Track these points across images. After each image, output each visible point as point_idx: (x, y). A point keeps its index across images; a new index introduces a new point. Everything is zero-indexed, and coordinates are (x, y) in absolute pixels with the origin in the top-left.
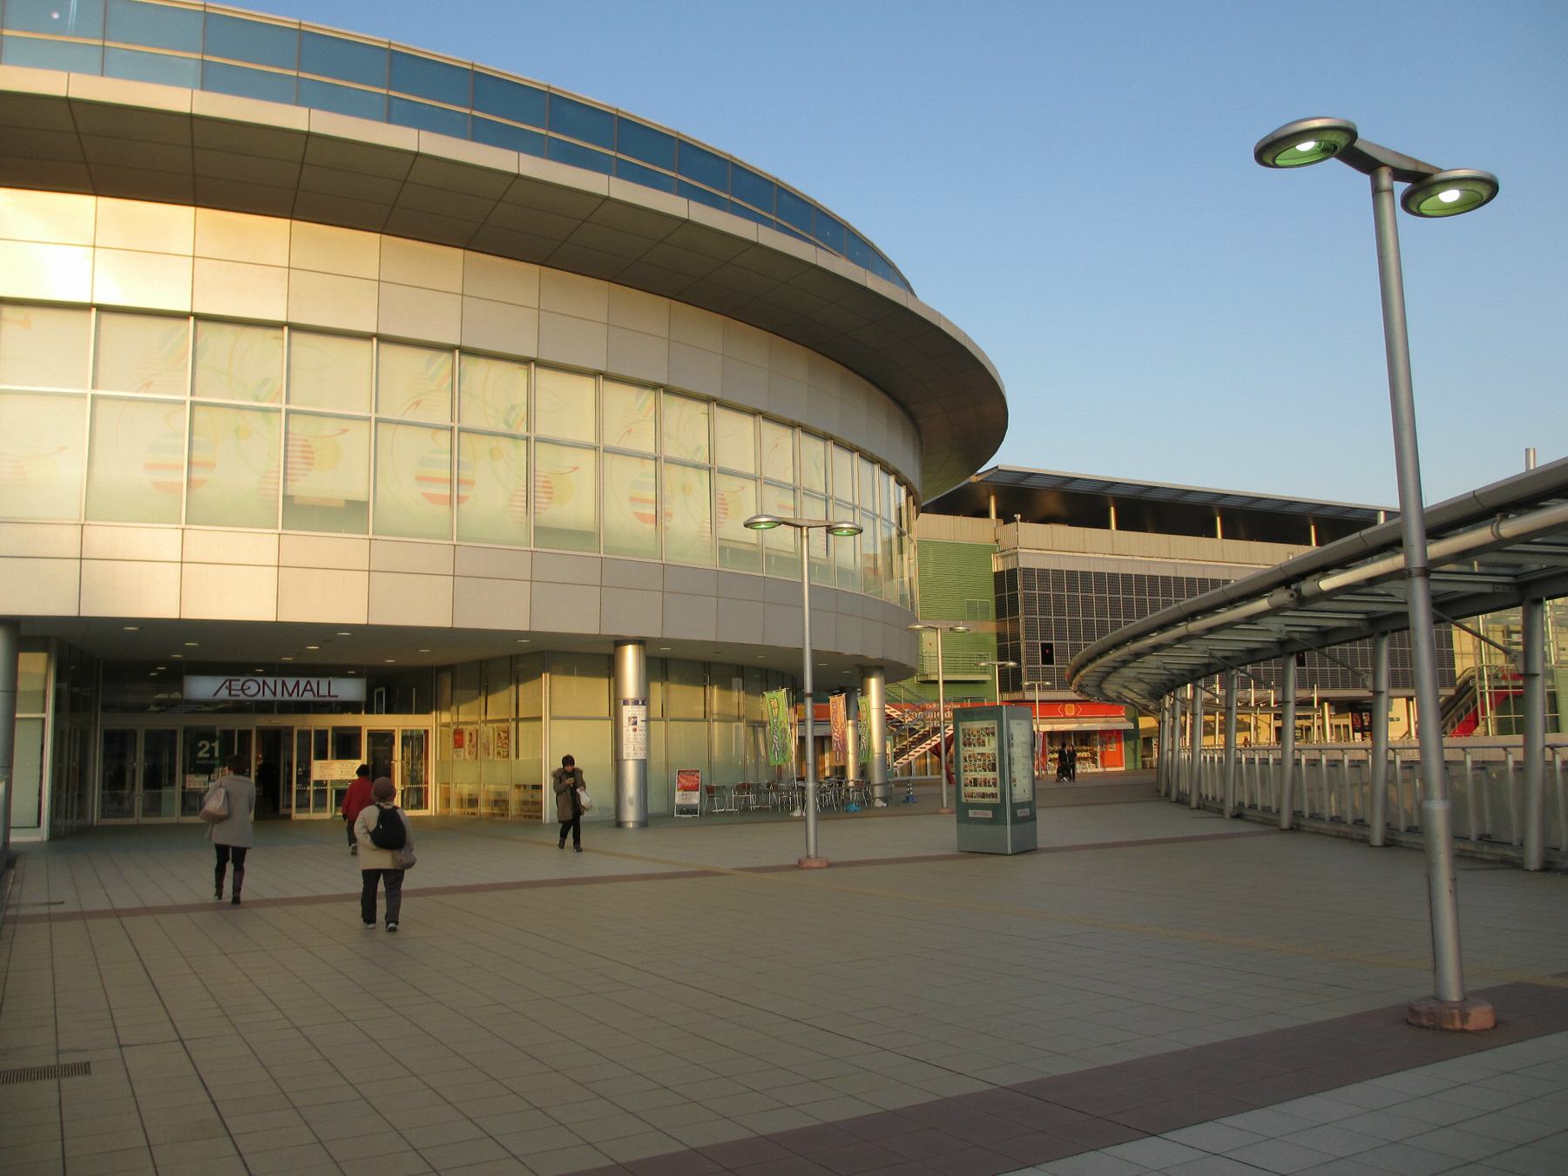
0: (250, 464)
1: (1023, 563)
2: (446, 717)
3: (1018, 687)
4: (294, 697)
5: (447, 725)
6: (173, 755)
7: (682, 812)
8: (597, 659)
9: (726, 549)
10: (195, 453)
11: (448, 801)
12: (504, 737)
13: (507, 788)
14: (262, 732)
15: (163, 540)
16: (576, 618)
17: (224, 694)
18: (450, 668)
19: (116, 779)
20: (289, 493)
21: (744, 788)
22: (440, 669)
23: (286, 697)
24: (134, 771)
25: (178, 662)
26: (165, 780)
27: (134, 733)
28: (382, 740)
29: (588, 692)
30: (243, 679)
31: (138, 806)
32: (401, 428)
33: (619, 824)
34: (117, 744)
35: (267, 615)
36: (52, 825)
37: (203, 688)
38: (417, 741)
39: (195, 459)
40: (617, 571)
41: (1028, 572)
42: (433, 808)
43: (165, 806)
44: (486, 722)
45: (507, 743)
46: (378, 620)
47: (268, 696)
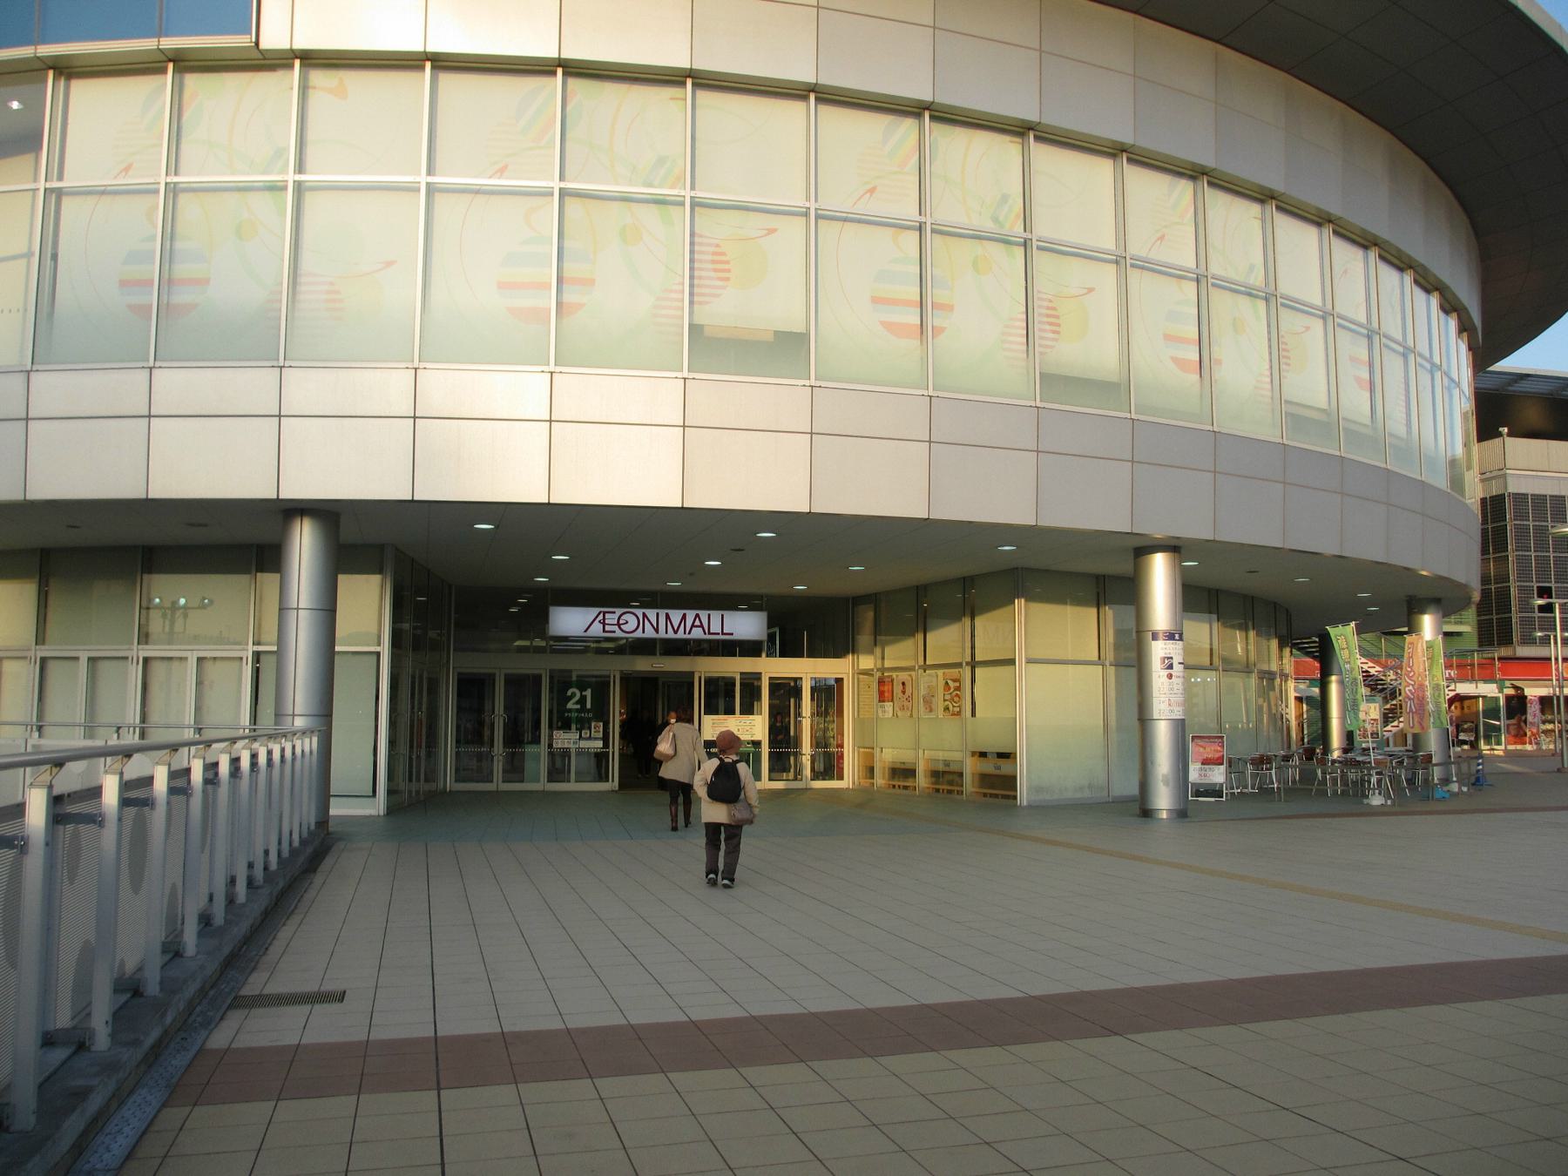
0: (636, 278)
1: (1513, 488)
2: (866, 662)
3: (1506, 640)
4: (681, 635)
5: (867, 673)
6: (537, 710)
7: (1198, 794)
8: (1098, 576)
9: (1296, 418)
10: (566, 265)
11: (871, 770)
12: (954, 690)
13: (956, 756)
14: (627, 679)
15: (519, 390)
16: (1094, 507)
17: (597, 630)
18: (872, 599)
19: (473, 733)
20: (697, 321)
21: (1261, 761)
22: (858, 600)
23: (671, 635)
24: (493, 725)
25: (542, 589)
26: (528, 736)
27: (492, 677)
28: (786, 691)
29: (1073, 629)
30: (619, 611)
31: (498, 767)
32: (848, 225)
33: (1147, 813)
34: (473, 689)
35: (669, 498)
36: (391, 792)
37: (571, 621)
38: (829, 695)
39: (566, 274)
40: (1156, 443)
41: (1520, 498)
42: (850, 777)
43: (529, 765)
44: (925, 667)
45: (957, 700)
46: (820, 508)
47: (649, 633)
